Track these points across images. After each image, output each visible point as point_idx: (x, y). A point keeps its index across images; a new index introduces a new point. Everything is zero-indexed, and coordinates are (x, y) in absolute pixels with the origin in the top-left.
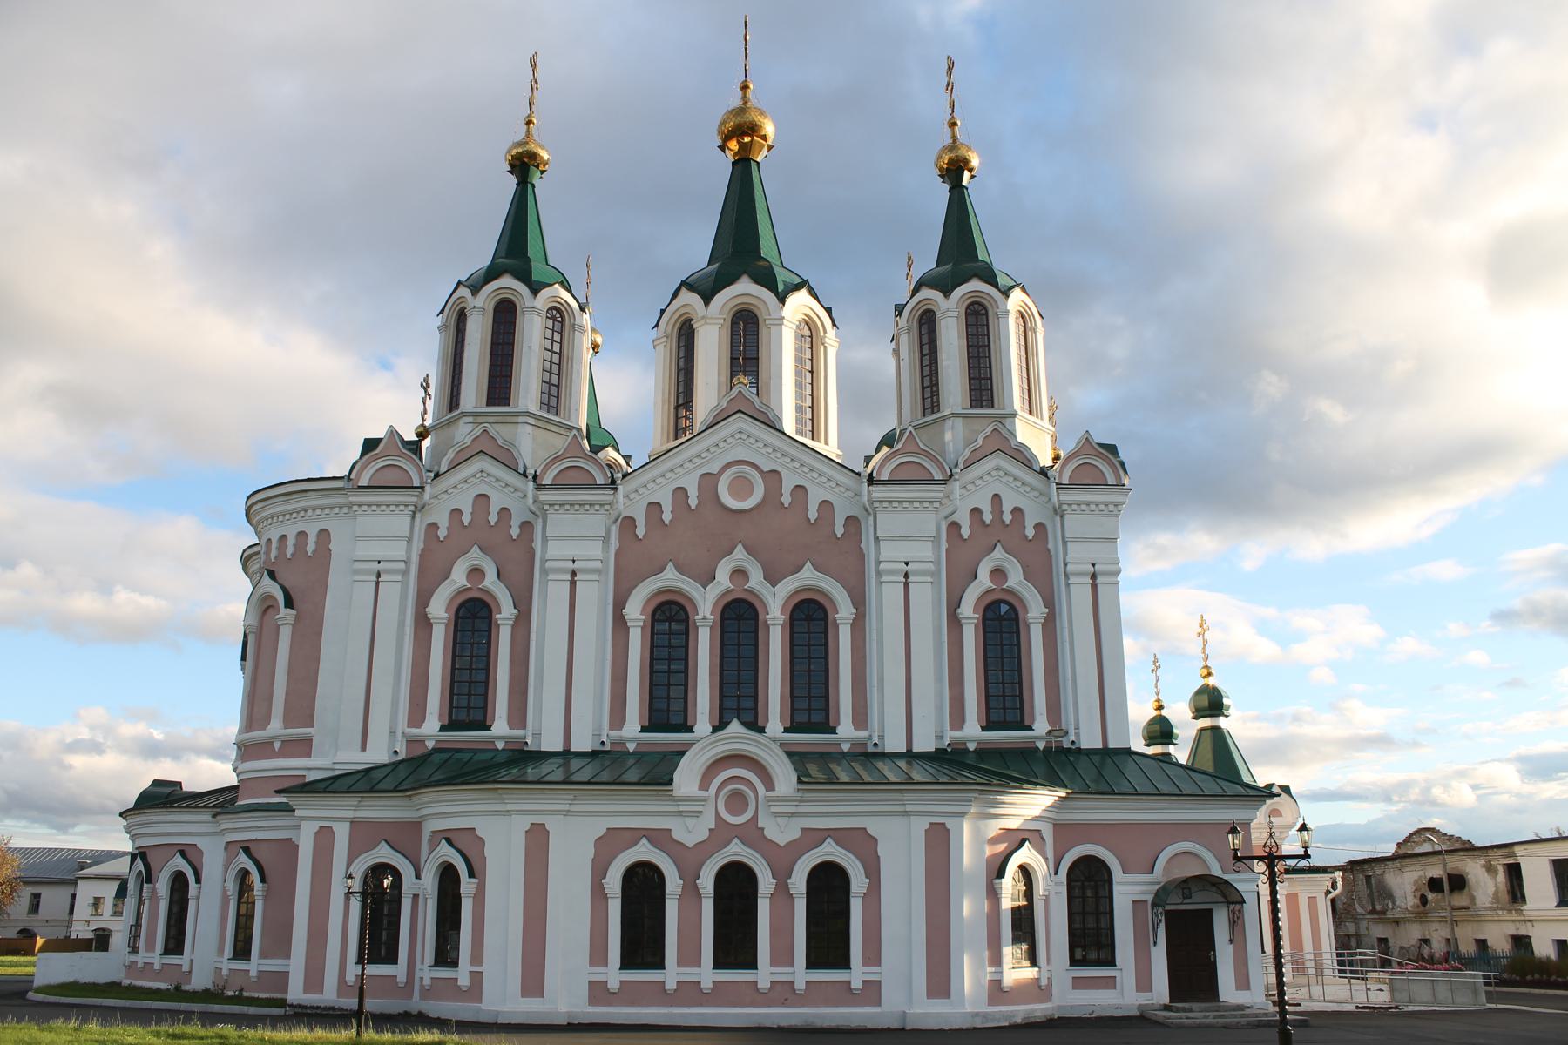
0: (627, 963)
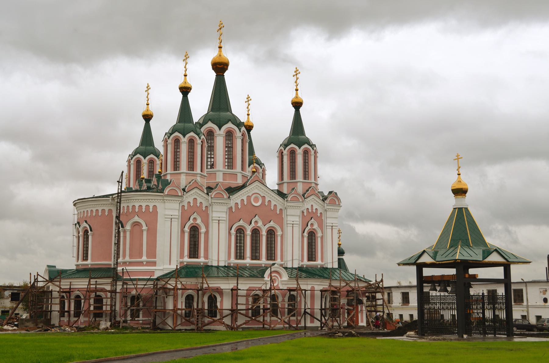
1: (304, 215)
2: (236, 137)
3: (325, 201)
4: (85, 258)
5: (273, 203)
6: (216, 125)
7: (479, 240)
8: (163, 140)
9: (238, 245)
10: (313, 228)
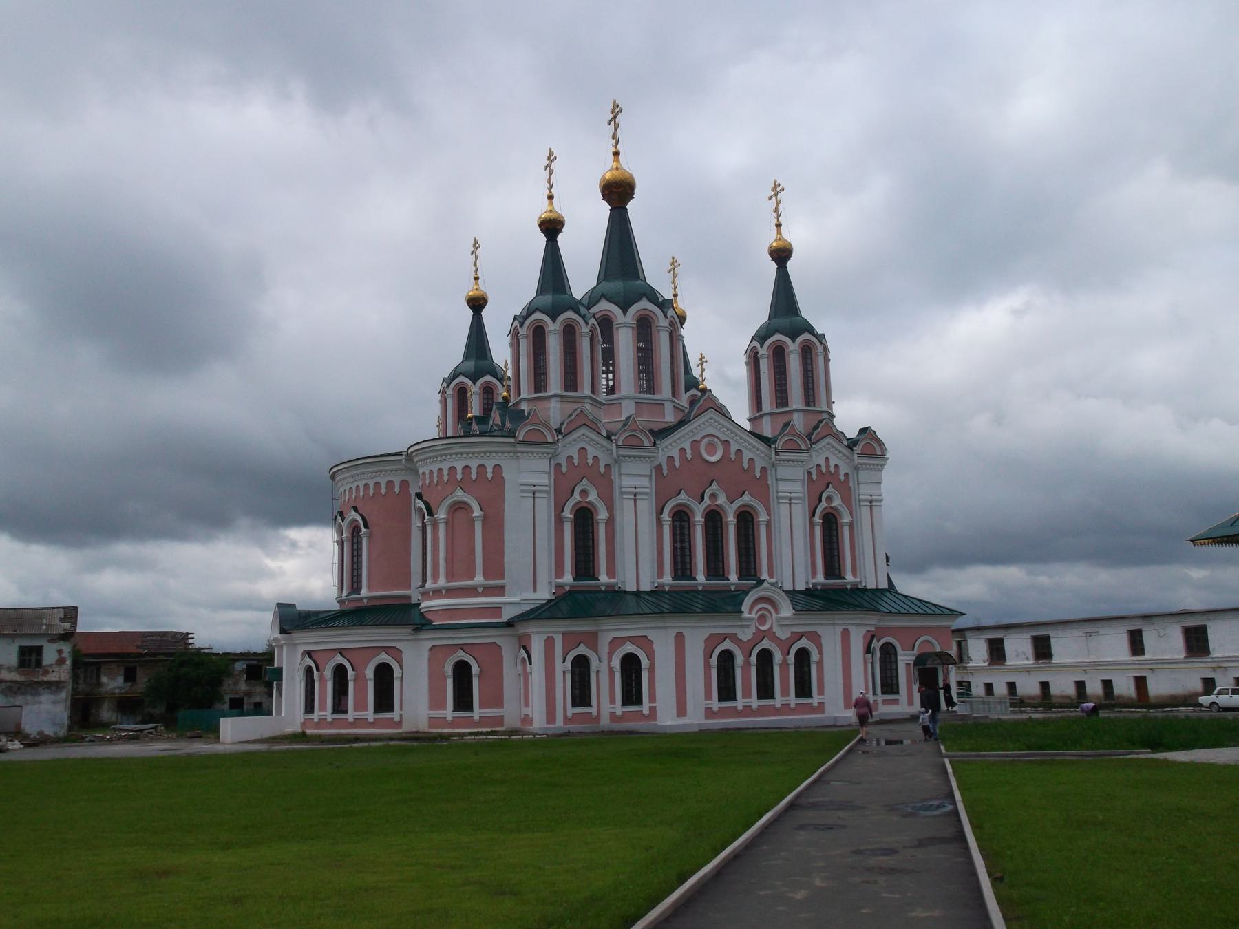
0: (721, 699)
1: (812, 479)
2: (658, 328)
3: (854, 449)
5: (747, 455)
8: (510, 333)
9: (678, 545)
10: (832, 506)
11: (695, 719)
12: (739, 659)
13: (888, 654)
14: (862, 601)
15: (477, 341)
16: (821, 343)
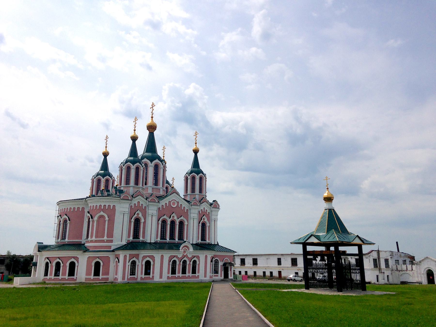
4: (64, 238)
5: (183, 206)
6: (149, 160)
7: (344, 230)
9: (162, 230)
10: (204, 221)
11: (164, 279)
12: (178, 263)
13: (217, 262)
14: (211, 248)
15: (105, 166)
16: (205, 176)
